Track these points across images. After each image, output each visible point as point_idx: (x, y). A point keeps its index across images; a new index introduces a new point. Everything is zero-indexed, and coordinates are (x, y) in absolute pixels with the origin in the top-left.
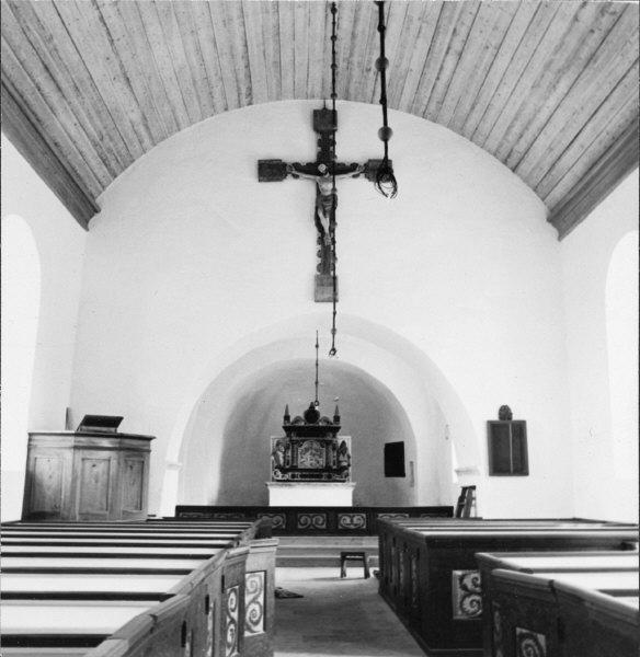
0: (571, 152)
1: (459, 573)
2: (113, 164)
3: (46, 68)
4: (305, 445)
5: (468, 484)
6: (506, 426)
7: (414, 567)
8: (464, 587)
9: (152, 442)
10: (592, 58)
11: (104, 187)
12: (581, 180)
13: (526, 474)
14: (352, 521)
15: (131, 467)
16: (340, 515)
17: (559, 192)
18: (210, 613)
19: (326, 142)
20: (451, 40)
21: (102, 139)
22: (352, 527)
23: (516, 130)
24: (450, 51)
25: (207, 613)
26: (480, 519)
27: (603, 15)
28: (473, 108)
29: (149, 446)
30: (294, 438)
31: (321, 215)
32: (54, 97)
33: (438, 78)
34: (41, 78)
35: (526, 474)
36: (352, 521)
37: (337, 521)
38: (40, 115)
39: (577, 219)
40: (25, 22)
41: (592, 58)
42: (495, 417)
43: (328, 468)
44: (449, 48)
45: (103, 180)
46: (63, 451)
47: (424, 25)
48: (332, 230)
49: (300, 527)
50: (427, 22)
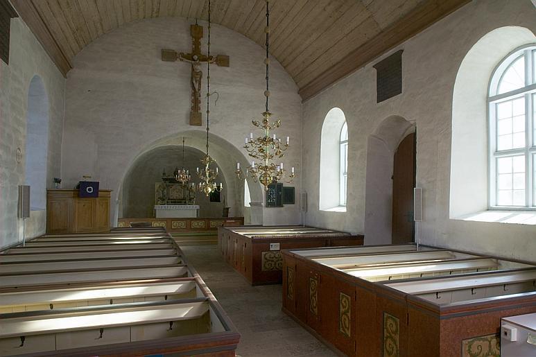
1: (263, 253)
2: (82, 43)
4: (173, 187)
5: (393, 102)
8: (266, 259)
11: (75, 55)
13: (363, 236)
19: (197, 44)
30: (168, 184)
31: (194, 82)
35: (363, 236)
43: (184, 199)
45: (75, 51)
48: (199, 90)
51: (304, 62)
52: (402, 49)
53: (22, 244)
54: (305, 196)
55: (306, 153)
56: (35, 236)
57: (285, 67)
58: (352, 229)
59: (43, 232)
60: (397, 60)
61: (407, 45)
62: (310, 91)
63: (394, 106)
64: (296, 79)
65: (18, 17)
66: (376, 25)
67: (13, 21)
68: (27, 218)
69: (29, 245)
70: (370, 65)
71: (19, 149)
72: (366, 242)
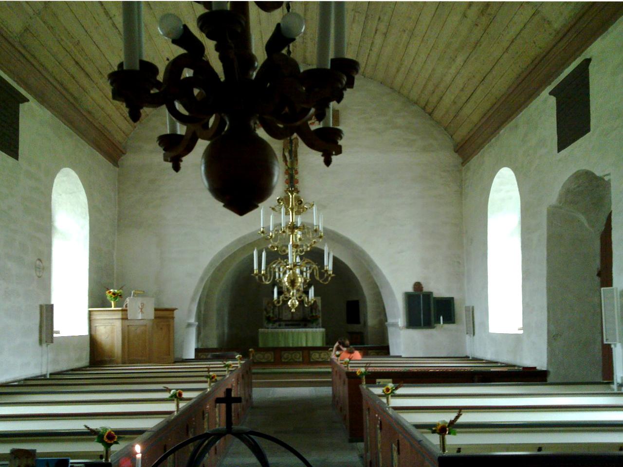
0: (468, 105)
3: (77, 63)
6: (419, 296)
7: (218, 419)
9: (175, 312)
10: (477, 43)
12: (485, 115)
14: (320, 356)
15: (161, 328)
16: (311, 352)
17: (462, 132)
18: (206, 419)
20: (378, 24)
21: (170, 390)
22: (320, 360)
23: (430, 87)
24: (378, 32)
25: (204, 419)
26: (400, 357)
27: (483, 15)
28: (398, 71)
29: (173, 314)
32: (85, 82)
33: (371, 50)
34: (74, 70)
36: (320, 356)
37: (309, 356)
38: (76, 95)
39: (474, 152)
40: (59, 36)
41: (477, 43)
42: (410, 289)
44: (376, 30)
46: (114, 321)
47: (357, 14)
49: (283, 360)
50: (358, 12)
51: (454, 103)
52: (588, 57)
53: (45, 376)
54: (471, 311)
55: (465, 239)
56: (69, 368)
57: (430, 114)
58: (535, 357)
59: (87, 364)
60: (582, 76)
61: (594, 50)
62: (467, 144)
63: (583, 155)
64: (447, 129)
65: (28, 100)
66: (546, 26)
67: (23, 108)
68: (52, 344)
69: (53, 377)
70: (545, 93)
71: (39, 260)
72: (550, 379)
